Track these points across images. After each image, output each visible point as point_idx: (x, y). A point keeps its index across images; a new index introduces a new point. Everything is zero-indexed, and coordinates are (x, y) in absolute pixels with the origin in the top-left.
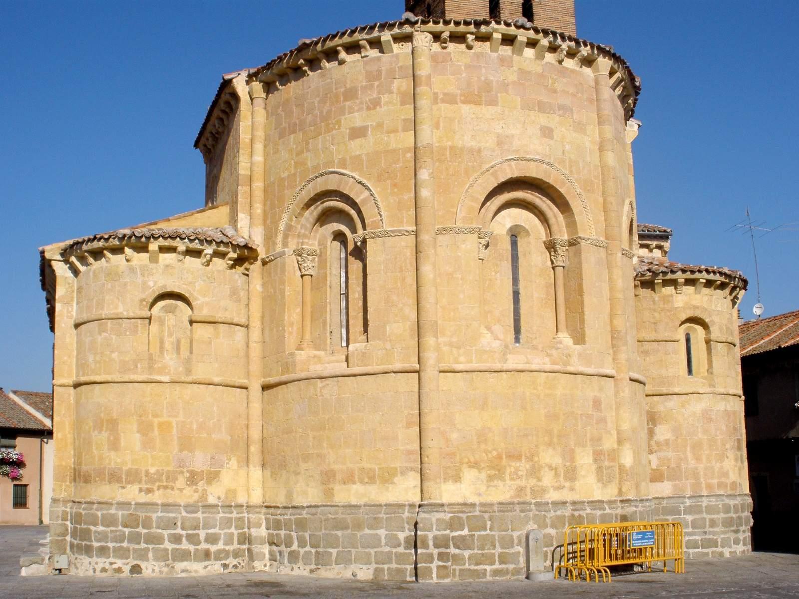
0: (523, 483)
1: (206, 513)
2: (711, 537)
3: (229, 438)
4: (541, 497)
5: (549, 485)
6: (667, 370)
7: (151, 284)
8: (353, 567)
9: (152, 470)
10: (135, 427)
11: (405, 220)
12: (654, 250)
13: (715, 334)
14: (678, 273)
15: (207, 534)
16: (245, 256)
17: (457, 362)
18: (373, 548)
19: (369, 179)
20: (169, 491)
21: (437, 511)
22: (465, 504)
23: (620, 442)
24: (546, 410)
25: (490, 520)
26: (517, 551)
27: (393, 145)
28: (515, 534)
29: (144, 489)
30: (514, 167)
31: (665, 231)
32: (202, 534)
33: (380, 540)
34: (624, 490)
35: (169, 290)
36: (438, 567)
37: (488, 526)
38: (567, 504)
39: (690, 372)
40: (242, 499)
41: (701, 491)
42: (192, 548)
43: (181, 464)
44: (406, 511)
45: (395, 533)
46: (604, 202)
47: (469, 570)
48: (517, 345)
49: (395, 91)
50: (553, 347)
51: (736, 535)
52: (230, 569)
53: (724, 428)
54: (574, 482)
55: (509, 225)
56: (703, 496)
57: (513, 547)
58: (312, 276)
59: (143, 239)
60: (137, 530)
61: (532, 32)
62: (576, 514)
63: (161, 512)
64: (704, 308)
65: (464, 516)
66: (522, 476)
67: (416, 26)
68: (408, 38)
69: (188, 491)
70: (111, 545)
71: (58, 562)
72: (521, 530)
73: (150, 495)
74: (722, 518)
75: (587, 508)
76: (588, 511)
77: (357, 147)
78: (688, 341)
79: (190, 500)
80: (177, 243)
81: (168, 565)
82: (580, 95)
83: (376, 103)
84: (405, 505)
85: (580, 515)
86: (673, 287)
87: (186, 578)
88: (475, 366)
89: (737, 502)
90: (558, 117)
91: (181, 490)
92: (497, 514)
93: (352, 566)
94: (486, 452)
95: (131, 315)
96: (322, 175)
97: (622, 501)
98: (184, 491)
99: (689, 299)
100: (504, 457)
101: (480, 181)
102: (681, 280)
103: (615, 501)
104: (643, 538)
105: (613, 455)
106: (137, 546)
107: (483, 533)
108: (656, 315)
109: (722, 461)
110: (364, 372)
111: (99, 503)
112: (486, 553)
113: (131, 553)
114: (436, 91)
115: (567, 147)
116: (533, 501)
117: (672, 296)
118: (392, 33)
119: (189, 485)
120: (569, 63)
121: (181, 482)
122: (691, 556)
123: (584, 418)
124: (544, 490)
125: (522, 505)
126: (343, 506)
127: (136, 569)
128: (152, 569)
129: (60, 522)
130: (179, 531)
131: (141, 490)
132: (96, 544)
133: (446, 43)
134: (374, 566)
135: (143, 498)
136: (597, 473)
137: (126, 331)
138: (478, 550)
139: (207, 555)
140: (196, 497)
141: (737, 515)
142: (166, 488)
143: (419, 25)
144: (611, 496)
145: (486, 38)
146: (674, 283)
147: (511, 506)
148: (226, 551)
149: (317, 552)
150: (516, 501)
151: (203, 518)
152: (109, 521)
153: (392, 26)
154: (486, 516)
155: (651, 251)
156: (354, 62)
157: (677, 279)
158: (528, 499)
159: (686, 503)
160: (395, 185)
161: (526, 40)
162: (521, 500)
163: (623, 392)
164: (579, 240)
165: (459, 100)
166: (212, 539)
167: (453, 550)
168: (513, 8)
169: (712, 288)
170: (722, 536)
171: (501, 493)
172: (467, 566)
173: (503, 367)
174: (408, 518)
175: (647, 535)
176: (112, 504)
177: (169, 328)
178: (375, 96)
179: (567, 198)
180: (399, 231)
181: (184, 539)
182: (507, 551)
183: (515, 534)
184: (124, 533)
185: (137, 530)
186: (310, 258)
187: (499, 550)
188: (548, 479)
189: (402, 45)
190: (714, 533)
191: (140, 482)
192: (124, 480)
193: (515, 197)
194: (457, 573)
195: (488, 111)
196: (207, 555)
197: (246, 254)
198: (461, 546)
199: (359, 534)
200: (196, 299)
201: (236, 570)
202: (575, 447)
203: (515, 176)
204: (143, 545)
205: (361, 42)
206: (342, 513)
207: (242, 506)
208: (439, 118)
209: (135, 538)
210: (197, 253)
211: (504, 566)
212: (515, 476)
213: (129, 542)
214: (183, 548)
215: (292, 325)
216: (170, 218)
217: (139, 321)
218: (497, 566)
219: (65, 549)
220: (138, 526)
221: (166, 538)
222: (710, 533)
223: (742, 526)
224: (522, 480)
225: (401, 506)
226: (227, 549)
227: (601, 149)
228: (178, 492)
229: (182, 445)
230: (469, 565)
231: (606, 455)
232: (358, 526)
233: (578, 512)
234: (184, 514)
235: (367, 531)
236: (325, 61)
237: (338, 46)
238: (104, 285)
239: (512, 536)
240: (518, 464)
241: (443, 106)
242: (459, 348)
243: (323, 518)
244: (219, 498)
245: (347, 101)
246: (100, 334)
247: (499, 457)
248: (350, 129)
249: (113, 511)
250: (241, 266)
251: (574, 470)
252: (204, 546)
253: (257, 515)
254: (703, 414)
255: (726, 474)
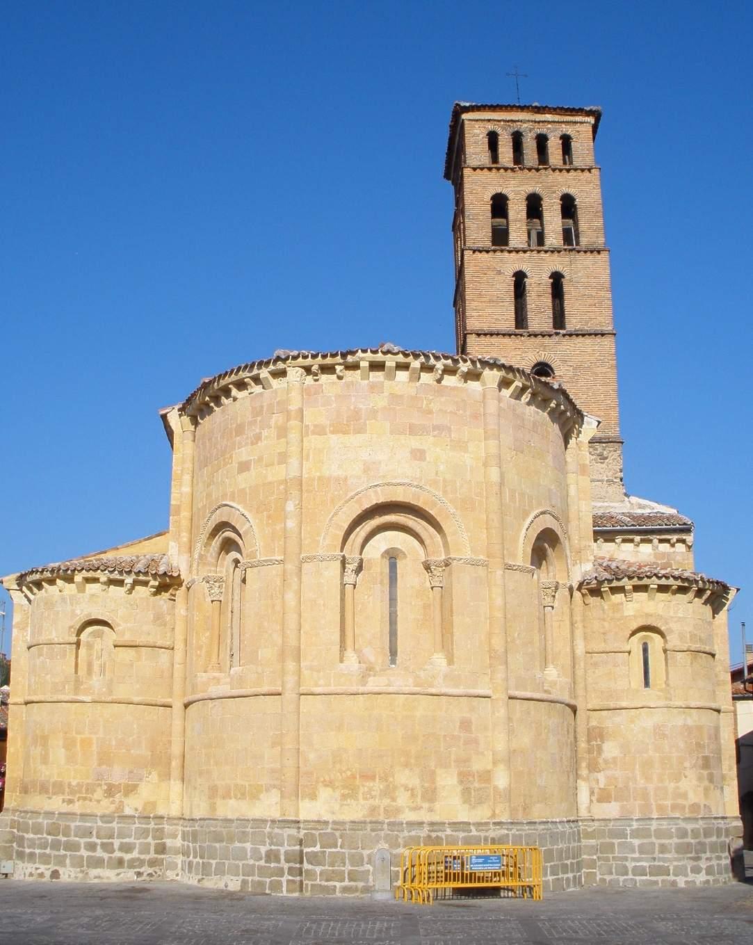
0: (377, 802)
1: (120, 823)
2: (661, 864)
3: (150, 753)
4: (395, 817)
5: (404, 805)
6: (616, 683)
7: (78, 612)
8: (227, 878)
9: (74, 783)
10: (61, 743)
11: (276, 549)
12: (676, 545)
13: (673, 641)
14: (623, 580)
15: (121, 843)
16: (168, 583)
17: (317, 685)
18: (241, 860)
19: (250, 511)
20: (87, 802)
21: (288, 827)
22: (319, 822)
23: (495, 763)
24: (403, 732)
25: (341, 838)
26: (367, 869)
27: (270, 479)
28: (366, 853)
29: (66, 800)
30: (380, 492)
31: (685, 524)
32: (117, 843)
33: (246, 854)
34: (497, 812)
35: (93, 618)
36: (288, 881)
37: (339, 844)
38: (424, 825)
39: (647, 684)
40: (161, 811)
41: (651, 813)
42: (106, 856)
43: (100, 777)
44: (268, 826)
45: (258, 846)
46: (487, 520)
47: (320, 885)
48: (393, 666)
49: (273, 425)
50: (421, 668)
51: (695, 863)
52: (144, 877)
53: (682, 745)
54: (434, 802)
55: (384, 548)
56: (653, 819)
57: (362, 865)
58: (221, 601)
59: (69, 572)
60: (58, 838)
61: (401, 356)
62: (434, 835)
63: (79, 821)
64: (658, 615)
65: (317, 833)
66: (375, 796)
67: (287, 362)
68: (283, 373)
69: (105, 802)
70: (37, 851)
71: (4, 867)
72: (372, 849)
73: (71, 805)
74: (675, 844)
75: (448, 830)
76: (449, 832)
77: (244, 481)
78: (645, 650)
79: (106, 811)
80: (98, 574)
81: (82, 872)
82: (461, 412)
83: (258, 438)
84: (267, 821)
85: (437, 836)
86: (623, 595)
87: (98, 883)
88: (332, 689)
89: (697, 826)
90: (432, 438)
91: (98, 801)
92: (348, 832)
93: (225, 877)
94: (341, 772)
95: (61, 641)
96: (219, 508)
97: (494, 823)
98: (101, 802)
99: (638, 607)
100: (358, 776)
101: (345, 509)
102: (629, 587)
103: (487, 824)
104: (484, 863)
105: (486, 776)
106: (57, 853)
107: (333, 850)
108: (606, 624)
109: (678, 780)
110: (240, 694)
111: (32, 812)
112: (336, 870)
113: (52, 859)
114: (307, 423)
115: (442, 468)
116: (386, 821)
117: (622, 604)
118: (268, 370)
119: (106, 797)
120: (449, 380)
121: (99, 794)
122: (638, 884)
123: (448, 739)
124: (398, 810)
125: (374, 825)
126: (221, 820)
127: (55, 874)
128: (69, 875)
129: (8, 829)
130: (94, 839)
131: (64, 801)
132: (28, 851)
133: (317, 376)
134: (241, 877)
135: (65, 808)
136: (463, 794)
137: (57, 655)
138: (329, 866)
139: (120, 863)
140: (112, 808)
141: (697, 840)
142: (85, 799)
143: (290, 361)
144: (482, 819)
145: (355, 367)
146: (621, 589)
147: (363, 825)
148: (141, 860)
149: (203, 863)
150: (368, 820)
151: (118, 828)
152: (37, 829)
153: (268, 363)
154: (338, 834)
155: (673, 545)
156: (243, 399)
157: (624, 586)
158: (381, 818)
159: (632, 825)
160: (269, 517)
161: (395, 365)
162: (374, 819)
163: (498, 712)
164: (450, 561)
165: (328, 431)
166: (127, 848)
167: (306, 866)
168: (541, 289)
169: (670, 594)
170: (675, 863)
171: (355, 811)
172: (318, 882)
173: (358, 689)
174: (269, 833)
175: (492, 859)
176: (40, 813)
177: (97, 652)
178: (258, 431)
179: (438, 520)
180: (271, 561)
181: (99, 847)
182: (356, 868)
183: (366, 853)
184: (48, 840)
185: (58, 838)
186: (217, 584)
187: (348, 867)
188: (403, 799)
189: (281, 380)
190: (664, 860)
191: (63, 794)
192: (51, 791)
193: (385, 521)
194: (309, 889)
195: (353, 439)
196: (120, 863)
197: (168, 581)
198: (313, 862)
199: (231, 847)
200: (118, 625)
201: (152, 879)
202: (436, 768)
203: (380, 502)
204: (62, 852)
205: (245, 380)
206: (221, 827)
207: (163, 818)
208: (309, 450)
209: (56, 845)
210: (120, 583)
211: (352, 883)
212: (369, 795)
213: (51, 849)
214: (98, 855)
215: (200, 648)
216: (119, 547)
217: (68, 646)
218: (346, 883)
219: (12, 855)
220: (59, 835)
221: (82, 846)
222: (660, 860)
223: (705, 852)
224: (375, 800)
225: (264, 821)
226: (142, 858)
227: (485, 465)
228: (95, 803)
229: (101, 759)
230: (320, 881)
231: (476, 777)
232: (231, 839)
233: (435, 833)
234: (100, 823)
235: (237, 844)
236: (223, 397)
237: (229, 384)
238: (43, 613)
239: (362, 855)
240: (372, 785)
241: (312, 437)
242: (319, 671)
243: (207, 830)
244: (136, 810)
245: (238, 436)
246: (39, 658)
247: (354, 777)
248: (238, 463)
249: (40, 820)
250: (167, 592)
251: (434, 790)
252: (118, 854)
253: (174, 827)
254: (654, 730)
255: (684, 796)
